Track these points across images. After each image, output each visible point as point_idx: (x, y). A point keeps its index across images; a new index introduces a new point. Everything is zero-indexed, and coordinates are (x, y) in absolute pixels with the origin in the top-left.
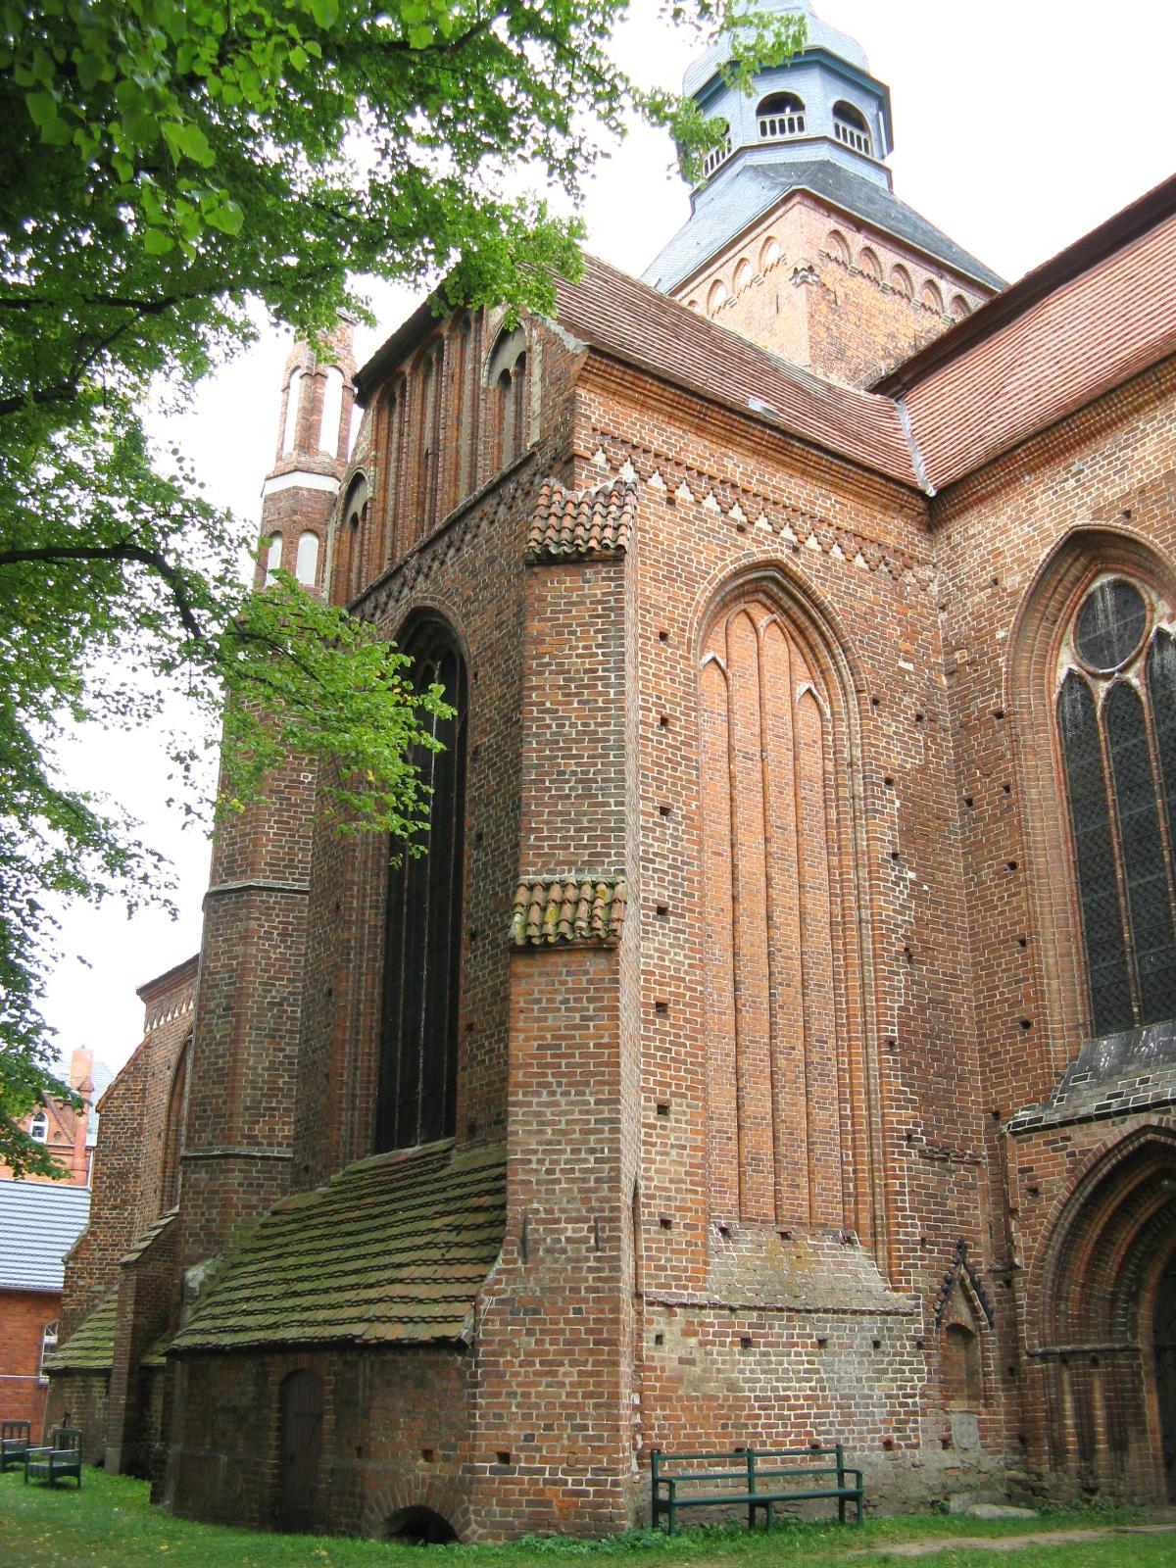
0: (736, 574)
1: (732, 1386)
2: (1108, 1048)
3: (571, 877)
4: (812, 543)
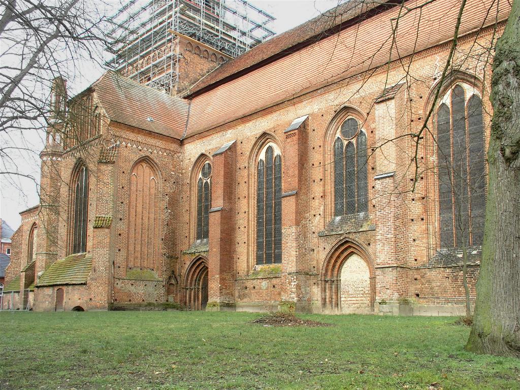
0: (139, 159)
1: (129, 291)
2: (199, 241)
3: (104, 216)
4: (155, 152)
